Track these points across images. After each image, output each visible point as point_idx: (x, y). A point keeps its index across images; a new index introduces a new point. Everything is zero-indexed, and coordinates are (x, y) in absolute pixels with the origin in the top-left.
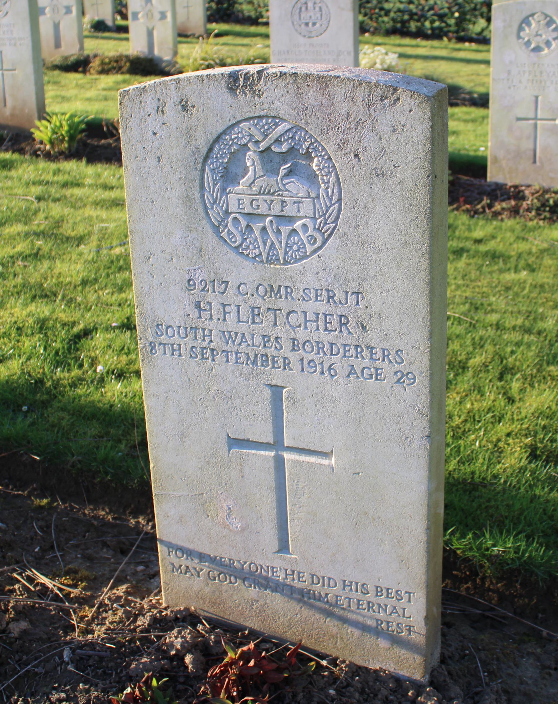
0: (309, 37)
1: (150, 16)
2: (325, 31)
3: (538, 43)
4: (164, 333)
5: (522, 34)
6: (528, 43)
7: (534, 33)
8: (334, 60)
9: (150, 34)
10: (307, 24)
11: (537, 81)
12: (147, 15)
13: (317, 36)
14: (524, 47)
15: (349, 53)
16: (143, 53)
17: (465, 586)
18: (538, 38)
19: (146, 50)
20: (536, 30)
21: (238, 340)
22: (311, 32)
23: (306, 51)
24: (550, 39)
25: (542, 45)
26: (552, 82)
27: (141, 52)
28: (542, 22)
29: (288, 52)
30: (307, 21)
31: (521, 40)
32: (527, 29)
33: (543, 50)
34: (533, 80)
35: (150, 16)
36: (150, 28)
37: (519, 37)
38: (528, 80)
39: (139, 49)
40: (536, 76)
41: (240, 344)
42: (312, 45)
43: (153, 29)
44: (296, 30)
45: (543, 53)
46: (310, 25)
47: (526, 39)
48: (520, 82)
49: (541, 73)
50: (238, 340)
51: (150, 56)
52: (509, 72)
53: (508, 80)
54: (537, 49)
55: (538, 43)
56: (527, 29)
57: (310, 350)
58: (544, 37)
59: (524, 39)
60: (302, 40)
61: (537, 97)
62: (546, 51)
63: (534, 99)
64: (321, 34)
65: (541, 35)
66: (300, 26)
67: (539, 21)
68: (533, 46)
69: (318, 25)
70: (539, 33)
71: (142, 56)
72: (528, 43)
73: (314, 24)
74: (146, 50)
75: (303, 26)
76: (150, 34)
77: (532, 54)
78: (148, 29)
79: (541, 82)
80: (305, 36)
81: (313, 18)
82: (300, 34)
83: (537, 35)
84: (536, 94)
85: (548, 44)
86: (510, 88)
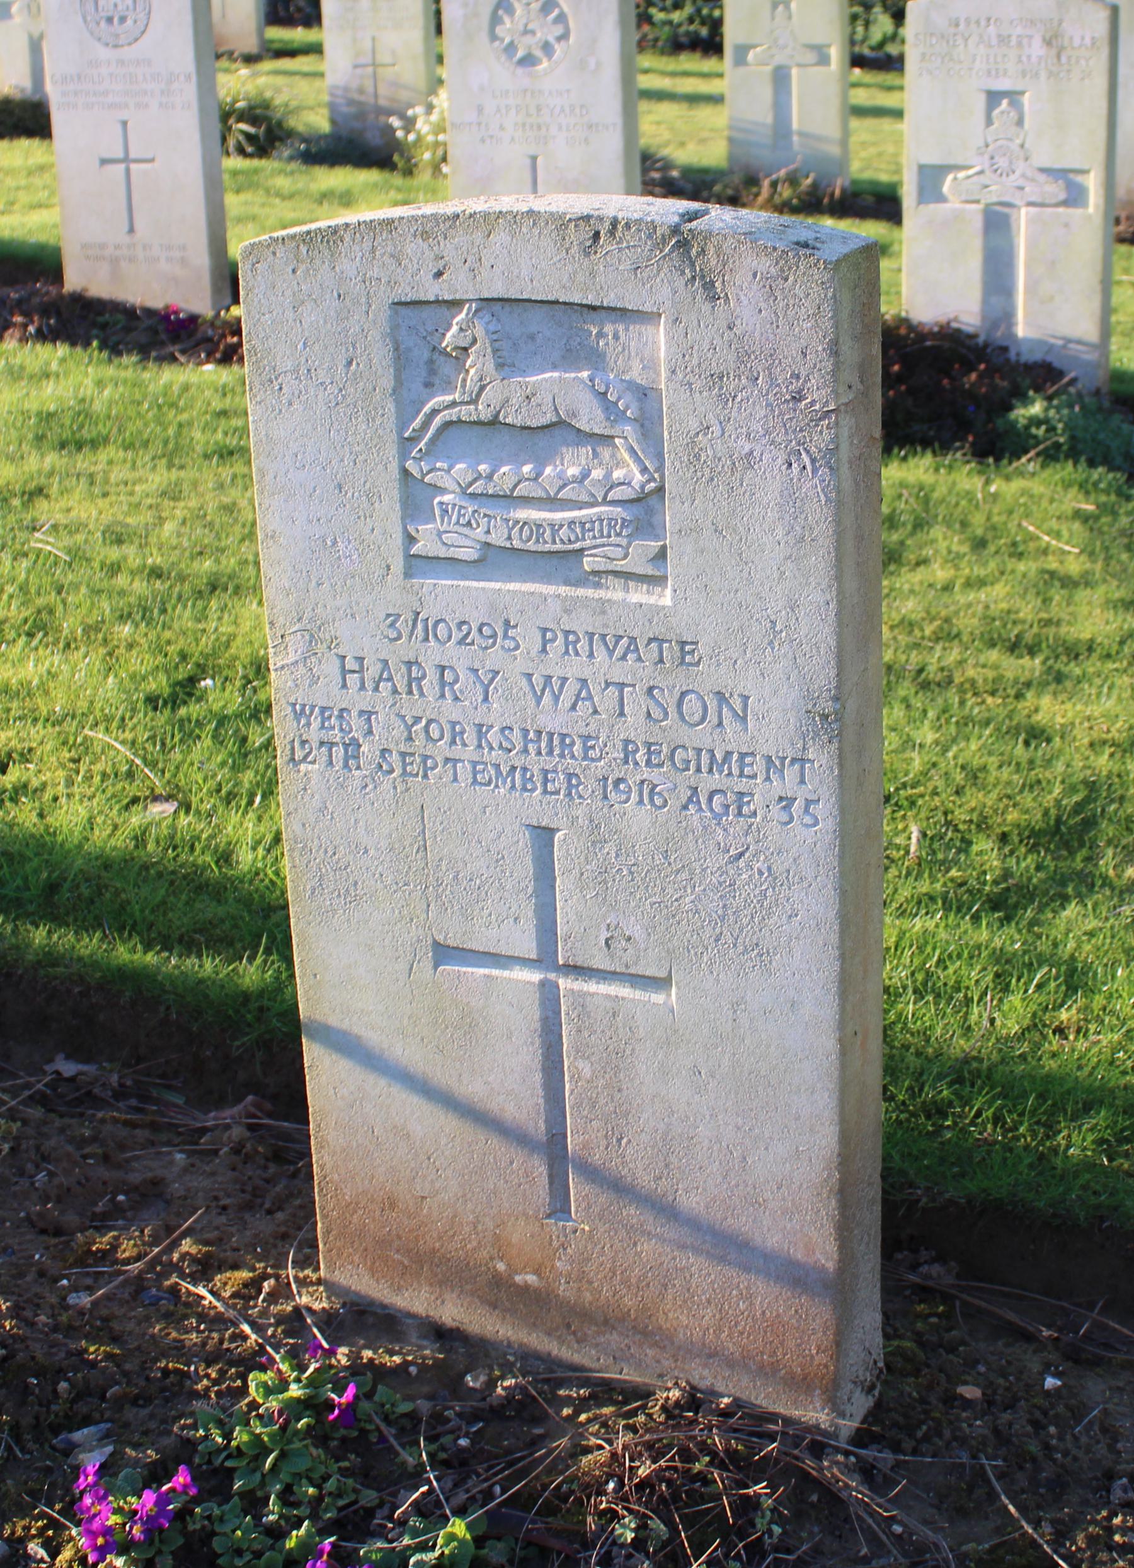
0: (116, 46)
1: (34, 9)
2: (143, 32)
3: (530, 47)
4: (672, 710)
5: (499, 30)
6: (511, 48)
7: (521, 28)
8: (162, 92)
9: (35, 48)
10: (110, 20)
11: (532, 126)
12: (29, 7)
13: (130, 44)
14: (503, 58)
15: (188, 78)
16: (23, 90)
17: (68, 1068)
18: (528, 40)
19: (27, 83)
20: (524, 21)
21: (566, 700)
22: (117, 36)
23: (111, 75)
24: (551, 39)
25: (538, 53)
26: (560, 128)
27: (16, 87)
28: (533, 6)
29: (79, 77)
30: (110, 14)
31: (497, 43)
32: (507, 20)
33: (539, 62)
34: (524, 125)
35: (34, 9)
36: (36, 34)
37: (493, 37)
38: (516, 124)
39: (14, 82)
40: (528, 115)
41: (573, 707)
42: (121, 62)
43: (41, 37)
44: (92, 34)
45: (540, 68)
46: (116, 20)
47: (507, 40)
48: (502, 128)
49: (539, 109)
50: (566, 700)
51: (37, 98)
52: (480, 110)
53: (479, 124)
54: (528, 61)
55: (530, 47)
56: (507, 20)
57: (697, 717)
58: (539, 35)
59: (502, 40)
60: (103, 53)
61: (534, 159)
62: (545, 64)
63: (528, 161)
64: (136, 40)
65: (533, 33)
66: (98, 23)
67: (528, 4)
68: (520, 54)
69: (129, 22)
70: (530, 27)
71: (18, 96)
72: (511, 48)
73: (123, 20)
74: (27, 83)
75: (103, 24)
76: (35, 48)
77: (520, 71)
78: (31, 38)
79: (539, 127)
80: (107, 45)
81: (120, 8)
82: (99, 39)
83: (526, 32)
84: (532, 152)
85: (547, 48)
86: (483, 141)
